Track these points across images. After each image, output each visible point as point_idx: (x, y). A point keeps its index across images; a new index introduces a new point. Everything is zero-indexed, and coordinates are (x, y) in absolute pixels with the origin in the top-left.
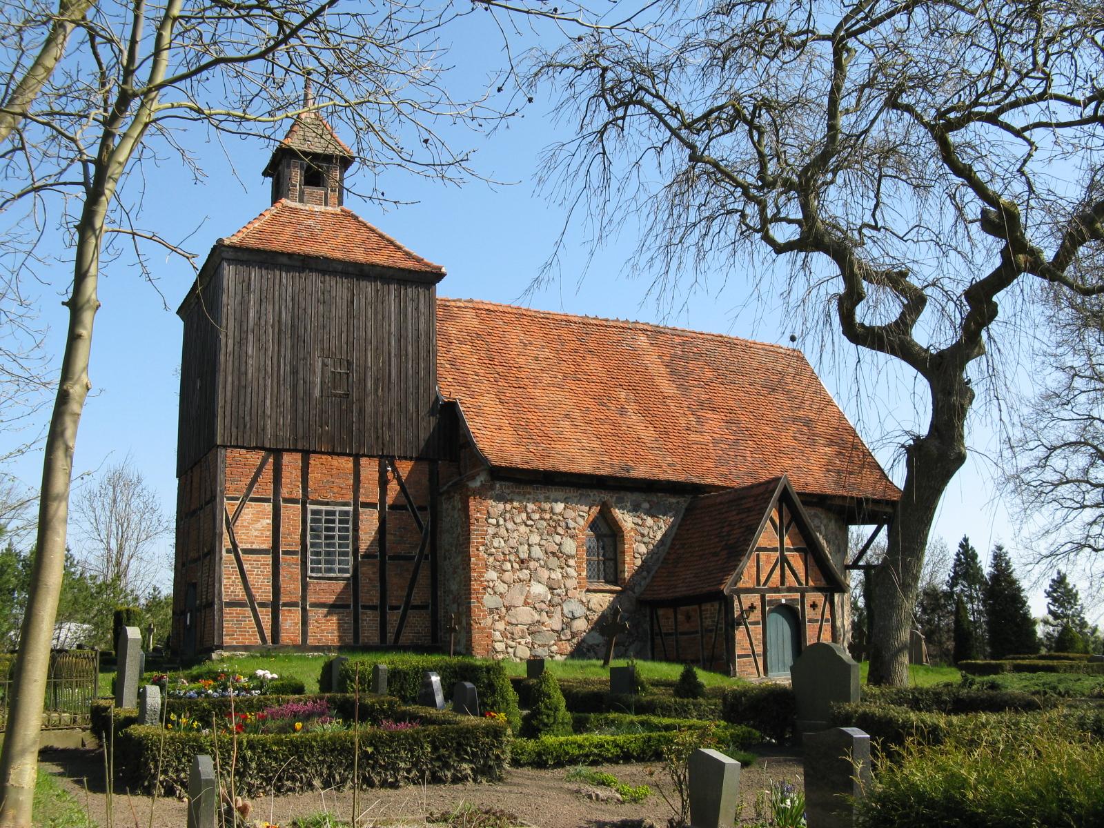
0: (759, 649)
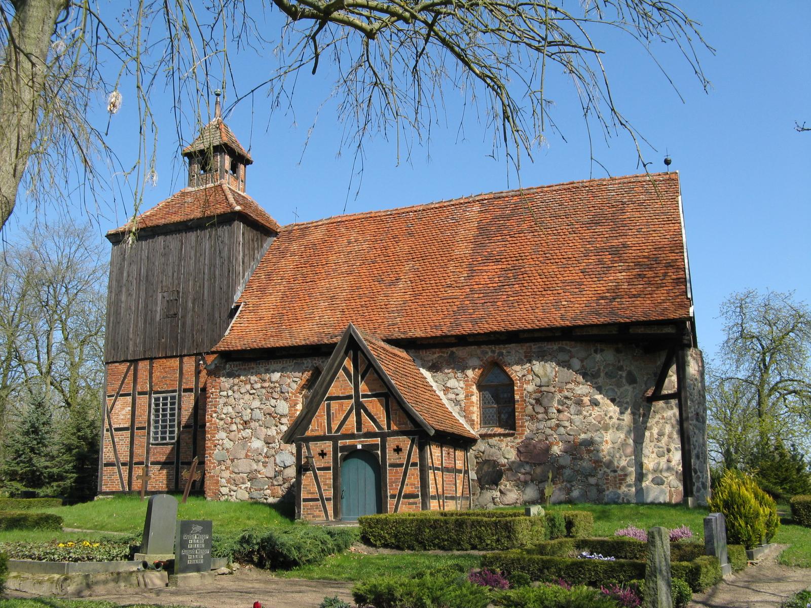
0: (329, 493)
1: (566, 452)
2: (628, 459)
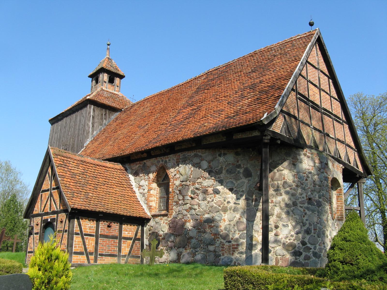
1: (194, 227)
2: (241, 233)
